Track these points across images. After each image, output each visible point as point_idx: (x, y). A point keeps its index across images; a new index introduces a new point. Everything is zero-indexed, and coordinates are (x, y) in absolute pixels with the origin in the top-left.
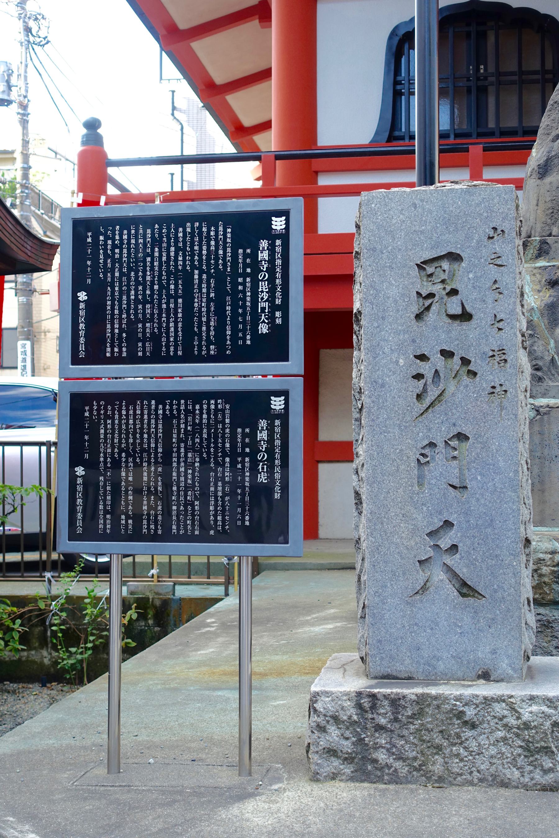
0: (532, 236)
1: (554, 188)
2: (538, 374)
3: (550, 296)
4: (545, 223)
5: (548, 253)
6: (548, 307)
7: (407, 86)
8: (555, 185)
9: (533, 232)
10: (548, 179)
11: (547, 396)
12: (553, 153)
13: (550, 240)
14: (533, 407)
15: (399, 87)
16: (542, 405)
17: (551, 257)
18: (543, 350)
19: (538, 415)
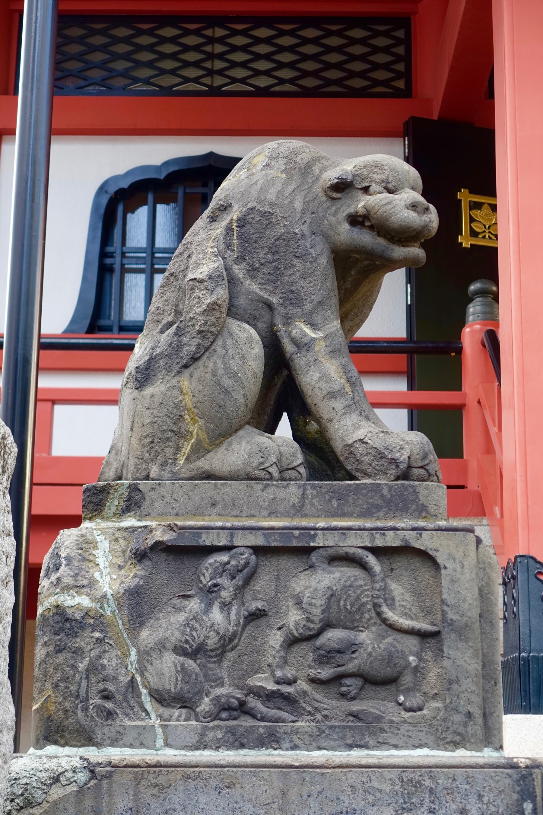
0: (124, 478)
1: (156, 405)
2: (106, 705)
3: (135, 576)
4: (140, 458)
5: (139, 507)
6: (130, 594)
7: (118, 259)
8: (157, 399)
9: (124, 472)
10: (149, 391)
11: (121, 743)
12: (158, 351)
13: (143, 485)
14: (86, 765)
15: (108, 261)
16: (100, 761)
17: (144, 513)
18: (117, 664)
19: (91, 779)
